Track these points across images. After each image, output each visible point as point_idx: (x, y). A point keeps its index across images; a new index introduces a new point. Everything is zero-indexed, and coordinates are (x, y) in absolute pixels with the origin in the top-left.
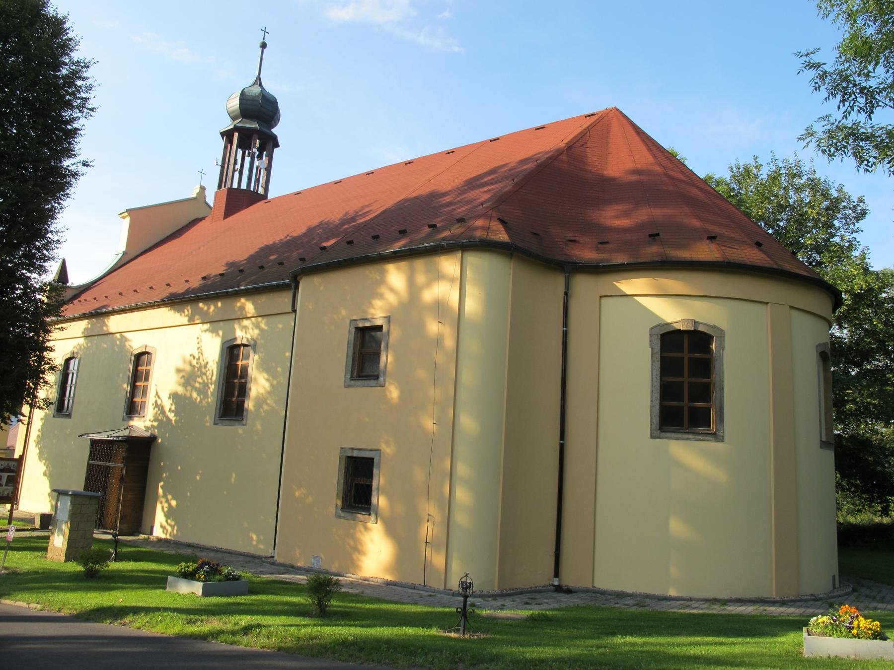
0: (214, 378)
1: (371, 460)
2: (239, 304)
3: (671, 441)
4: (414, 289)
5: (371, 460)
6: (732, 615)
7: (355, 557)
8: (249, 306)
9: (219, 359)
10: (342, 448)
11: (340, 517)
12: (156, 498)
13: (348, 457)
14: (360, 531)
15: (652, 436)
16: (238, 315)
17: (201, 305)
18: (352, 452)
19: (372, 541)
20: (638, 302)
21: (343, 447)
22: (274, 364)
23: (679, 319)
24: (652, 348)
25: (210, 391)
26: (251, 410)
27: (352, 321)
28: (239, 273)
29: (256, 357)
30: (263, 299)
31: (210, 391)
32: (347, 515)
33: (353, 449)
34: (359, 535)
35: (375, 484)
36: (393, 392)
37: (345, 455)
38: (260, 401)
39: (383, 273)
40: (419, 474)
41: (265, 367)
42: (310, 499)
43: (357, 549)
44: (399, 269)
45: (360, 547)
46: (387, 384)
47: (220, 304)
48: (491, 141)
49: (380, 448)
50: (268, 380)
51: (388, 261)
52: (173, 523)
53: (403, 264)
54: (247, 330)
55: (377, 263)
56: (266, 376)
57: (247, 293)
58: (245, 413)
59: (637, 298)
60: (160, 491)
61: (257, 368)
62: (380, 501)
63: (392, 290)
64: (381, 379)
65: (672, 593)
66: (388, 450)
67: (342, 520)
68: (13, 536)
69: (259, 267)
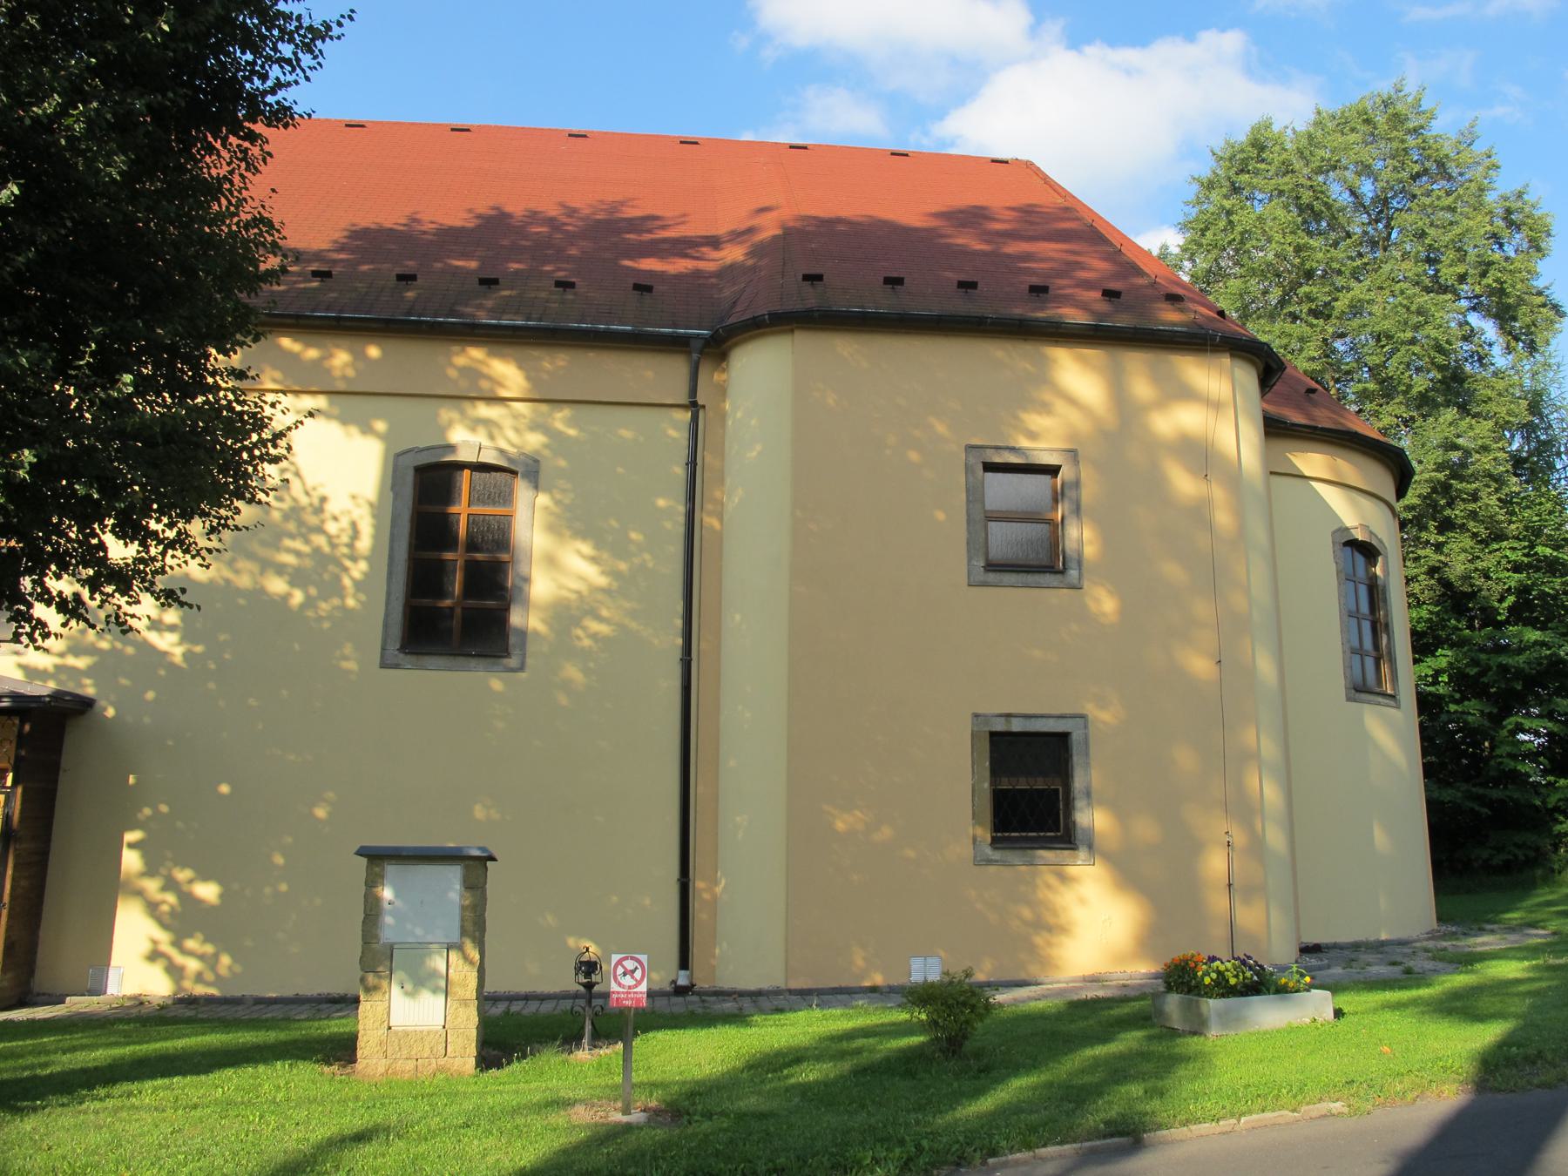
0: (365, 543)
1: (1064, 737)
2: (460, 361)
3: (1366, 706)
4: (1126, 410)
5: (1064, 737)
6: (73, 1072)
7: (1038, 940)
8: (507, 372)
9: (381, 494)
10: (976, 716)
11: (989, 862)
12: (111, 887)
13: (993, 734)
14: (1049, 887)
15: (1349, 699)
16: (463, 387)
17: (286, 342)
18: (1009, 722)
19: (1082, 901)
20: (1316, 491)
21: (980, 711)
22: (614, 523)
23: (1356, 524)
24: (1336, 563)
25: (353, 579)
26: (536, 633)
27: (970, 448)
28: (477, 286)
29: (543, 499)
30: (557, 362)
31: (353, 579)
32: (1012, 856)
33: (1008, 716)
34: (1043, 893)
35: (1078, 783)
36: (1104, 603)
37: (987, 729)
38: (566, 615)
39: (1045, 365)
40: (1185, 759)
41: (574, 522)
42: (887, 832)
43: (1049, 925)
44: (1084, 361)
45: (1051, 920)
46: (1086, 584)
47: (374, 352)
48: (994, 161)
49: (1085, 712)
50: (594, 560)
51: (1057, 342)
52: (209, 949)
53: (1093, 353)
54: (495, 432)
55: (946, 336)
56: (586, 548)
57: (498, 337)
58: (512, 640)
59: (1314, 484)
60: (131, 860)
61: (552, 529)
62: (1093, 818)
63: (1072, 401)
64: (1073, 573)
65: (1384, 937)
66: (1104, 716)
67: (992, 869)
68: (643, 988)
69: (635, 285)
